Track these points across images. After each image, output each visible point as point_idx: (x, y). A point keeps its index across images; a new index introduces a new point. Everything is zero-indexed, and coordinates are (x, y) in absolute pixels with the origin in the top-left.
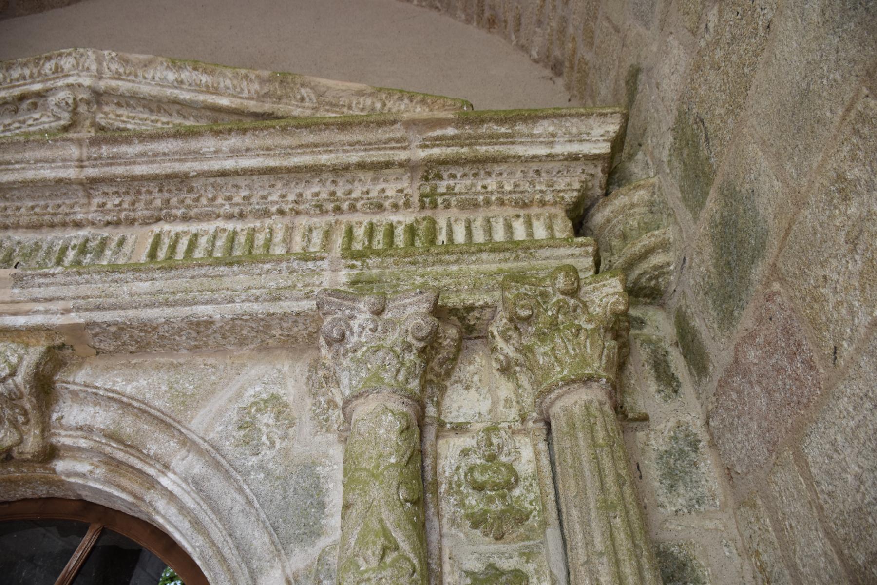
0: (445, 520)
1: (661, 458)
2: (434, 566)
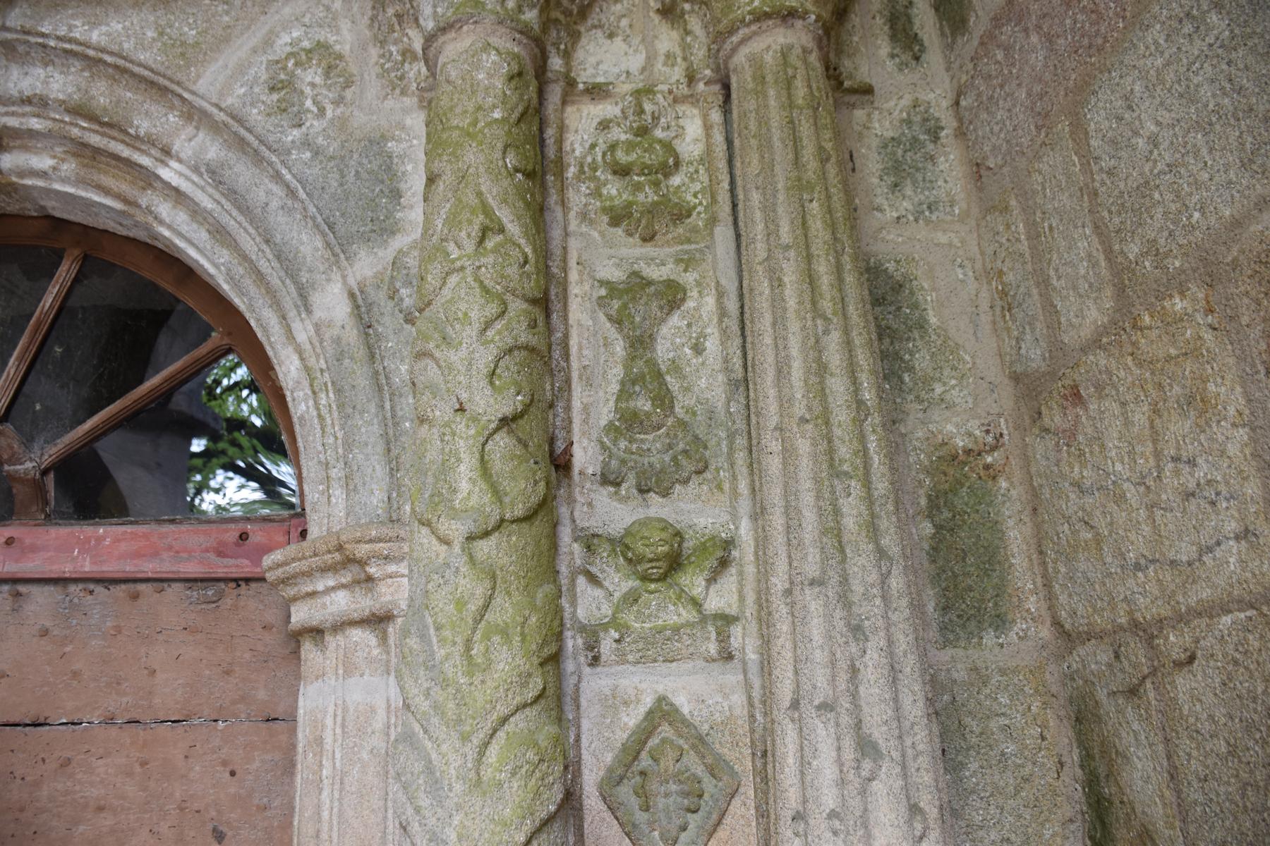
0: (572, 214)
1: (885, 146)
2: (555, 270)
